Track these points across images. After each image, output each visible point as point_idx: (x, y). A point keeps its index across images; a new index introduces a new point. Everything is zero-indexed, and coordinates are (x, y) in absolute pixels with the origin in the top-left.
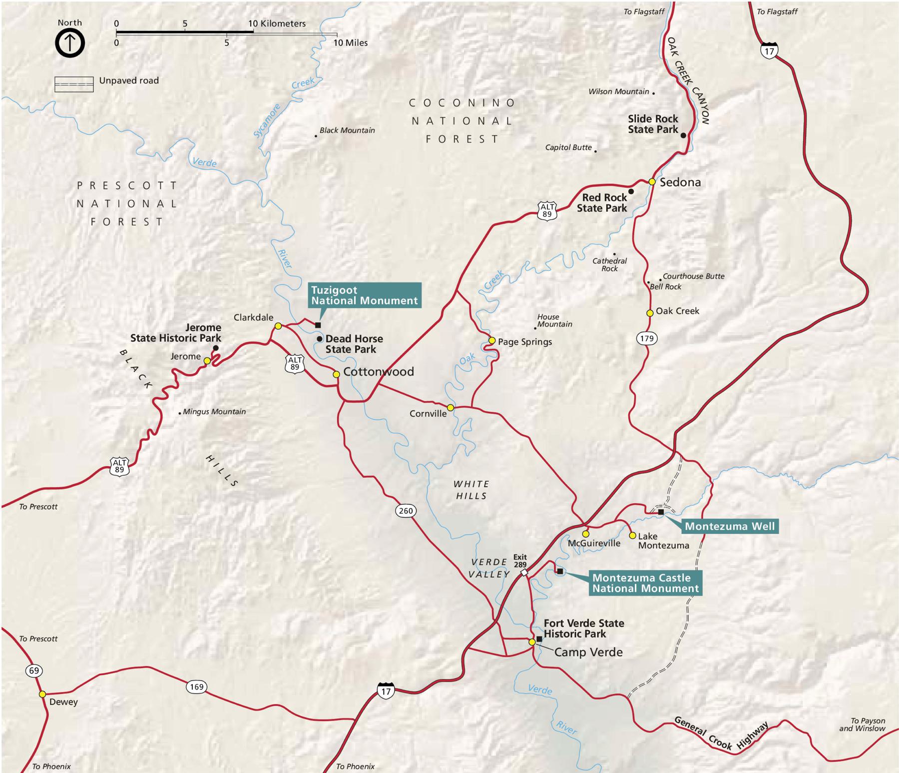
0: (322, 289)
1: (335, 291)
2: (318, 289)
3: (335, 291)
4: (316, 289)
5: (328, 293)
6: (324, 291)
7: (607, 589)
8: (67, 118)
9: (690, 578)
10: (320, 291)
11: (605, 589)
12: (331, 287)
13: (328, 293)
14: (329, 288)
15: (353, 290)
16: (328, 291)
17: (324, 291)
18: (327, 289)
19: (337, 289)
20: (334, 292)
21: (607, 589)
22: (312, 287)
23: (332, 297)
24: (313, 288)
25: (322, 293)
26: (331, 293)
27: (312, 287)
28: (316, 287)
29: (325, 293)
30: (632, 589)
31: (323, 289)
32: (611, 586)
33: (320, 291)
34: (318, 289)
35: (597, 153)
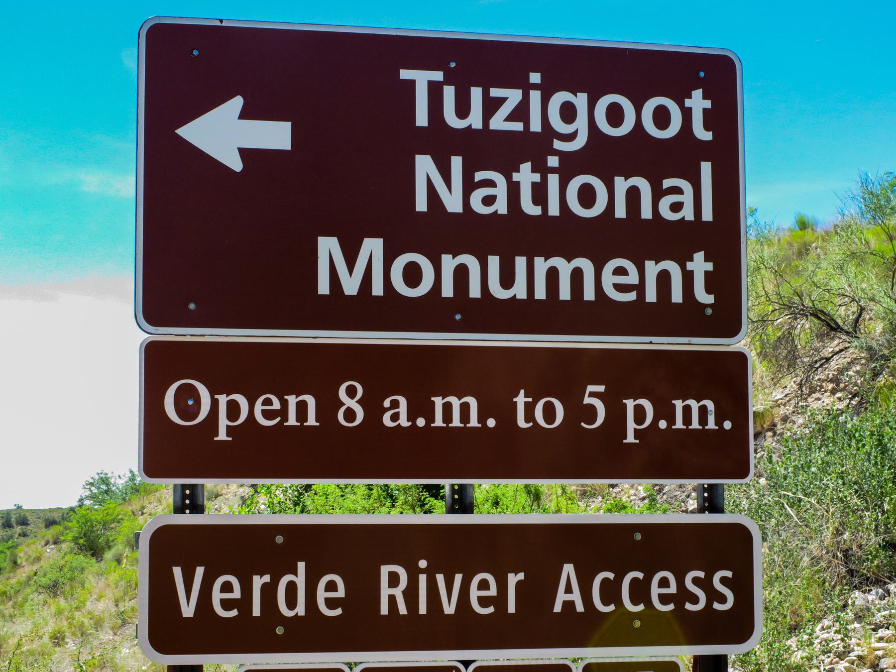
0: (476, 94)
1: (569, 114)
2: (449, 93)
3: (569, 114)
4: (435, 90)
5: (495, 92)
6: (491, 106)
7: (514, 190)
8: (688, 343)
9: (341, 593)
10: (463, 110)
11: (501, 191)
12: (535, 78)
13: (495, 92)
14: (527, 88)
15: (687, 114)
16: (521, 113)
17: (491, 106)
18: (514, 96)
19: (581, 101)
20: (558, 125)
21: (514, 190)
22: (405, 74)
23: (553, 161)
24: (412, 83)
25: (475, 120)
26: (536, 126)
27: (405, 74)
28: (438, 76)
29: (498, 123)
30: (687, 198)
31: (486, 94)
32: (540, 167)
33: (463, 110)
34: (449, 93)
35: (228, 483)
